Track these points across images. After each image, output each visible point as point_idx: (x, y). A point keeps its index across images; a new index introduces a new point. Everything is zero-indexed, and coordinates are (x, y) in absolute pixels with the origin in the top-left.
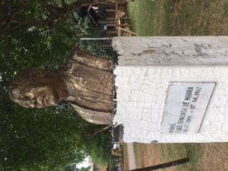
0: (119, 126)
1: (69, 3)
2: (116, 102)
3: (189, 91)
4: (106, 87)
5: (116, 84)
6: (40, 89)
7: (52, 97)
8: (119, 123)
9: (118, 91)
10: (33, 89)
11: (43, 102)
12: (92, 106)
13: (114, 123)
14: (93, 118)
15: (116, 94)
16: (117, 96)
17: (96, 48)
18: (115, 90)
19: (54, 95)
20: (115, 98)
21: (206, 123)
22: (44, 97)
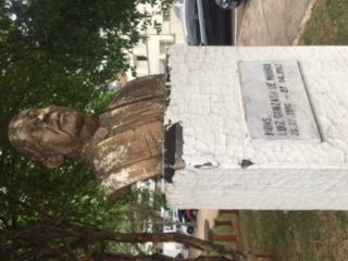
2: (168, 86)
3: (267, 68)
16: (171, 78)
20: (168, 80)
21: (323, 120)
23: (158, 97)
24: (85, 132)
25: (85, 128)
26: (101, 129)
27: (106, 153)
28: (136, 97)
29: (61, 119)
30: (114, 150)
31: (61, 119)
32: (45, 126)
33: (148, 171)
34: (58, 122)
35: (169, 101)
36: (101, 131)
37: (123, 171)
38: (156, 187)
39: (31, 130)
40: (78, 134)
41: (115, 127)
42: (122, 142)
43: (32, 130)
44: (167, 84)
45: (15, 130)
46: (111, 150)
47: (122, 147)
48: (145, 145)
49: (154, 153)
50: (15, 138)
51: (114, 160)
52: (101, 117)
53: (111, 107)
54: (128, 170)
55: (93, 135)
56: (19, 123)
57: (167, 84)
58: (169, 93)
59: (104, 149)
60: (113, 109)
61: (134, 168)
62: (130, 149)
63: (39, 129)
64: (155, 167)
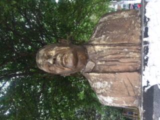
0: (152, 87)
1: (108, 101)
2: (146, 43)
4: (132, 34)
5: (147, 15)
6: (62, 48)
7: (72, 55)
8: (151, 84)
9: (150, 25)
10: (57, 47)
11: (62, 59)
12: (113, 68)
13: (144, 84)
14: (113, 91)
15: (147, 29)
16: (149, 33)
17: (116, 115)
18: (146, 23)
19: (74, 54)
20: (146, 36)
22: (64, 54)
25: (79, 63)
29: (64, 62)
30: (101, 82)
31: (64, 62)
33: (126, 103)
34: (62, 64)
35: (147, 60)
36: (90, 65)
41: (99, 63)
44: (145, 39)
45: (40, 65)
47: (107, 83)
48: (124, 87)
54: (113, 98)
57: (145, 39)
58: (147, 50)
60: (97, 45)
62: (112, 86)
64: (132, 102)
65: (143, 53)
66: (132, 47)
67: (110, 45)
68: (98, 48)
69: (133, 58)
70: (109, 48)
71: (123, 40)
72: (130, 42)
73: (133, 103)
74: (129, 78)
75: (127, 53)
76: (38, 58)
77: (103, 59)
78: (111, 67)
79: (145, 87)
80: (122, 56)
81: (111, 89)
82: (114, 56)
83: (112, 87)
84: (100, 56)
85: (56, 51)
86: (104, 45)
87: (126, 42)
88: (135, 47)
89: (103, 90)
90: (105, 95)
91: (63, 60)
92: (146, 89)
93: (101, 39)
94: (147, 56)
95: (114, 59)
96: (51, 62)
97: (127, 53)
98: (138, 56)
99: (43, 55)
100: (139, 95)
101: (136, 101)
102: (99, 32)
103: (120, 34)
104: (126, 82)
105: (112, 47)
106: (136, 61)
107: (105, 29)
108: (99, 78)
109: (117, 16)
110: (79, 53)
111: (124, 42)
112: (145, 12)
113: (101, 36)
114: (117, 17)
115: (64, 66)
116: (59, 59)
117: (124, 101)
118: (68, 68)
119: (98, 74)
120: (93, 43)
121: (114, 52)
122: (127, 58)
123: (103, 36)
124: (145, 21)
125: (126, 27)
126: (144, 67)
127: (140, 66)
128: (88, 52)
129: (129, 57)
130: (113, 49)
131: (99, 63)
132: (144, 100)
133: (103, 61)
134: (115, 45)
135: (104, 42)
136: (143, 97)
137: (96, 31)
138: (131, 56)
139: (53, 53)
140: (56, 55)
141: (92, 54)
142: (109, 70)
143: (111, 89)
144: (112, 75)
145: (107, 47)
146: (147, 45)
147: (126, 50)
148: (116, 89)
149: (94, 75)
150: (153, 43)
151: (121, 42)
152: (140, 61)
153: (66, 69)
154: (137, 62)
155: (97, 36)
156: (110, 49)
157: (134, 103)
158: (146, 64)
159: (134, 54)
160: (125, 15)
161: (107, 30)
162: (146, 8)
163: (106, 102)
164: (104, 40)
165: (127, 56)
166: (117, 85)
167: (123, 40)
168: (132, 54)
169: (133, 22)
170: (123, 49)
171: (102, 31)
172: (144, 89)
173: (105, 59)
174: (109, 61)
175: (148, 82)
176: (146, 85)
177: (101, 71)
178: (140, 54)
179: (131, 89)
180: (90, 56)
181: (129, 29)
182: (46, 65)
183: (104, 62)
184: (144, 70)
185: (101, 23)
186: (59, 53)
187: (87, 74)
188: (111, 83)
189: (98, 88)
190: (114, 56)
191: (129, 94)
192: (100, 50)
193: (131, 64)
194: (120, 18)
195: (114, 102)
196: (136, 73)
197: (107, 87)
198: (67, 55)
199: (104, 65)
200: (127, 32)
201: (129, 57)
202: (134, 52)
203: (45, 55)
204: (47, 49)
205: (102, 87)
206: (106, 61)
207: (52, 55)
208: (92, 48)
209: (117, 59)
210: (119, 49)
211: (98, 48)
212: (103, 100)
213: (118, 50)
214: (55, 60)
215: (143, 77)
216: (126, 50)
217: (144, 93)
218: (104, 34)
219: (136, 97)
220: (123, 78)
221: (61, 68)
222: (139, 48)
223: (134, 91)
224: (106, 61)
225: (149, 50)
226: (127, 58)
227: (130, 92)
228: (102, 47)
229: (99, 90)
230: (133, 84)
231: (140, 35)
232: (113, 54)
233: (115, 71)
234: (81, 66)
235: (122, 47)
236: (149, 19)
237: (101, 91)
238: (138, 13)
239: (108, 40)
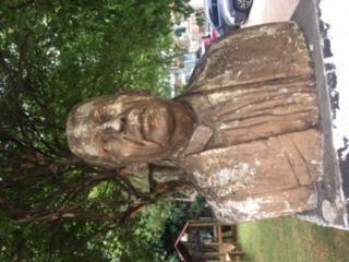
2: (329, 67)
4: (293, 61)
5: (324, 18)
9: (331, 34)
15: (327, 43)
16: (333, 49)
18: (324, 32)
20: (328, 54)
23: (300, 79)
24: (178, 135)
25: (178, 130)
26: (201, 128)
27: (214, 168)
28: (257, 74)
29: (146, 125)
30: (230, 167)
31: (146, 125)
32: (123, 135)
33: (292, 205)
34: (142, 130)
35: (336, 98)
36: (201, 134)
37: (250, 200)
38: (177, 80)
39: (103, 140)
40: (170, 141)
41: (224, 127)
42: (246, 157)
43: (105, 142)
44: (327, 61)
45: (78, 141)
46: (223, 165)
47: (245, 166)
48: (286, 166)
49: (304, 180)
50: (80, 151)
51: (231, 182)
52: (196, 102)
53: (209, 87)
54: (259, 200)
55: (189, 138)
56: (80, 130)
57: (327, 61)
58: (333, 80)
59: (210, 161)
60: (212, 91)
61: (269, 200)
62: (258, 170)
63: (112, 138)
64: (304, 200)
65: (328, 87)
66: (297, 84)
67: (248, 86)
68: (215, 97)
69: (301, 103)
70: (245, 91)
71: (275, 72)
72: (290, 75)
73: (305, 203)
74: (299, 146)
75: (288, 95)
76: (75, 123)
77: (232, 117)
78: (253, 129)
79: (341, 150)
80: (279, 102)
81: (255, 179)
82: (259, 106)
83: (261, 175)
84: (224, 108)
85: (124, 104)
86: (231, 88)
87: (283, 75)
88: (302, 84)
89: (238, 184)
90: (235, 196)
91: (146, 120)
92: (344, 154)
93: (222, 79)
94: (336, 89)
95: (259, 113)
96: (116, 126)
97: (288, 95)
98: (310, 99)
99: (92, 114)
100: (320, 179)
101: (312, 196)
102: (211, 67)
103: (267, 62)
104: (291, 155)
105: (252, 90)
106: (309, 108)
107: (230, 58)
108: (225, 161)
109: (251, 34)
110: (175, 109)
111: (278, 76)
112: (320, 15)
113: (223, 72)
114: (253, 36)
115: (145, 138)
116: (133, 118)
117: (286, 202)
118: (152, 141)
119: (224, 150)
120: (203, 88)
121: (256, 97)
122: (289, 104)
123: (227, 72)
124: (323, 29)
125: (278, 48)
126: (334, 112)
127: (317, 117)
128: (195, 107)
129: (294, 103)
130: (254, 93)
131: (224, 127)
132: (343, 177)
133: (234, 120)
134: (258, 84)
135: (233, 83)
136: (342, 171)
137: (206, 68)
138: (297, 100)
139: (117, 107)
140: (126, 112)
141: (205, 110)
142: (251, 136)
143: (255, 179)
144: (260, 145)
145: (239, 92)
146: (332, 71)
147: (285, 90)
148: (268, 175)
149: (211, 157)
150: (343, 65)
151: (272, 77)
152: (316, 108)
153: (148, 144)
154: (310, 110)
155: (210, 75)
156: (247, 94)
157: (309, 202)
158: (336, 106)
159: (304, 95)
160: (271, 32)
161: (235, 59)
162: (321, 6)
163: (243, 214)
164: (232, 78)
165: (289, 100)
166: (272, 166)
167: (275, 72)
168: (298, 96)
169: (290, 40)
170: (277, 90)
171: (222, 63)
172: (340, 155)
173: (239, 116)
174: (249, 117)
175: (346, 140)
176: (343, 146)
177: (230, 142)
178: (315, 95)
179: (304, 168)
180: (200, 116)
181: (285, 52)
182: (96, 137)
183: (236, 123)
184: (334, 117)
185: (215, 51)
186: (133, 108)
187: (196, 155)
188: (258, 163)
189: (222, 183)
190: (259, 106)
191: (298, 181)
192: (223, 100)
193: (297, 115)
194: (260, 38)
195: (264, 208)
196: (314, 133)
197: (248, 174)
198: (151, 111)
199: (237, 128)
200: (280, 57)
201: (294, 103)
202: (303, 92)
203: (96, 114)
204: (101, 102)
205: (234, 178)
206: (241, 119)
207: (112, 113)
208: (202, 98)
209: (267, 111)
210: (269, 91)
211: (215, 97)
212: (235, 211)
213: (266, 94)
214: (124, 121)
215: (334, 131)
216: (285, 90)
217: (342, 164)
218: (229, 69)
219: (310, 187)
220: (285, 147)
221: (136, 142)
222: (311, 84)
223: (308, 172)
224: (241, 119)
225: (338, 80)
226: (289, 104)
227: (300, 178)
228: (228, 94)
229: (226, 187)
230: (306, 157)
231: (309, 59)
232: (256, 103)
233: (263, 135)
234: (181, 137)
235: (275, 87)
236: (327, 25)
237: (230, 189)
238: (305, 24)
239: (242, 77)
